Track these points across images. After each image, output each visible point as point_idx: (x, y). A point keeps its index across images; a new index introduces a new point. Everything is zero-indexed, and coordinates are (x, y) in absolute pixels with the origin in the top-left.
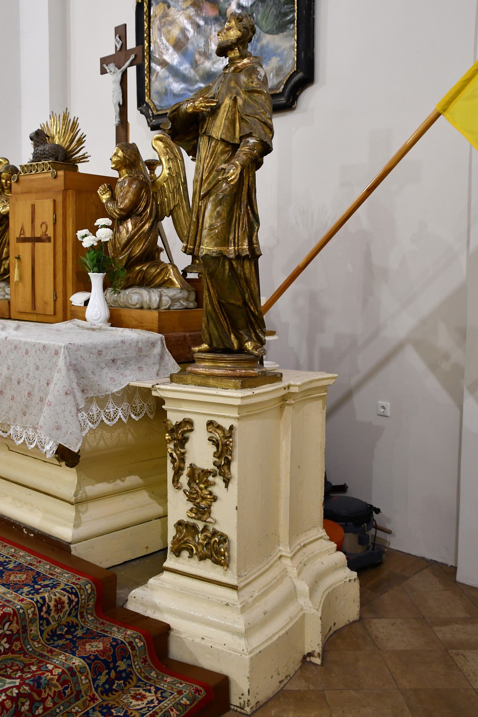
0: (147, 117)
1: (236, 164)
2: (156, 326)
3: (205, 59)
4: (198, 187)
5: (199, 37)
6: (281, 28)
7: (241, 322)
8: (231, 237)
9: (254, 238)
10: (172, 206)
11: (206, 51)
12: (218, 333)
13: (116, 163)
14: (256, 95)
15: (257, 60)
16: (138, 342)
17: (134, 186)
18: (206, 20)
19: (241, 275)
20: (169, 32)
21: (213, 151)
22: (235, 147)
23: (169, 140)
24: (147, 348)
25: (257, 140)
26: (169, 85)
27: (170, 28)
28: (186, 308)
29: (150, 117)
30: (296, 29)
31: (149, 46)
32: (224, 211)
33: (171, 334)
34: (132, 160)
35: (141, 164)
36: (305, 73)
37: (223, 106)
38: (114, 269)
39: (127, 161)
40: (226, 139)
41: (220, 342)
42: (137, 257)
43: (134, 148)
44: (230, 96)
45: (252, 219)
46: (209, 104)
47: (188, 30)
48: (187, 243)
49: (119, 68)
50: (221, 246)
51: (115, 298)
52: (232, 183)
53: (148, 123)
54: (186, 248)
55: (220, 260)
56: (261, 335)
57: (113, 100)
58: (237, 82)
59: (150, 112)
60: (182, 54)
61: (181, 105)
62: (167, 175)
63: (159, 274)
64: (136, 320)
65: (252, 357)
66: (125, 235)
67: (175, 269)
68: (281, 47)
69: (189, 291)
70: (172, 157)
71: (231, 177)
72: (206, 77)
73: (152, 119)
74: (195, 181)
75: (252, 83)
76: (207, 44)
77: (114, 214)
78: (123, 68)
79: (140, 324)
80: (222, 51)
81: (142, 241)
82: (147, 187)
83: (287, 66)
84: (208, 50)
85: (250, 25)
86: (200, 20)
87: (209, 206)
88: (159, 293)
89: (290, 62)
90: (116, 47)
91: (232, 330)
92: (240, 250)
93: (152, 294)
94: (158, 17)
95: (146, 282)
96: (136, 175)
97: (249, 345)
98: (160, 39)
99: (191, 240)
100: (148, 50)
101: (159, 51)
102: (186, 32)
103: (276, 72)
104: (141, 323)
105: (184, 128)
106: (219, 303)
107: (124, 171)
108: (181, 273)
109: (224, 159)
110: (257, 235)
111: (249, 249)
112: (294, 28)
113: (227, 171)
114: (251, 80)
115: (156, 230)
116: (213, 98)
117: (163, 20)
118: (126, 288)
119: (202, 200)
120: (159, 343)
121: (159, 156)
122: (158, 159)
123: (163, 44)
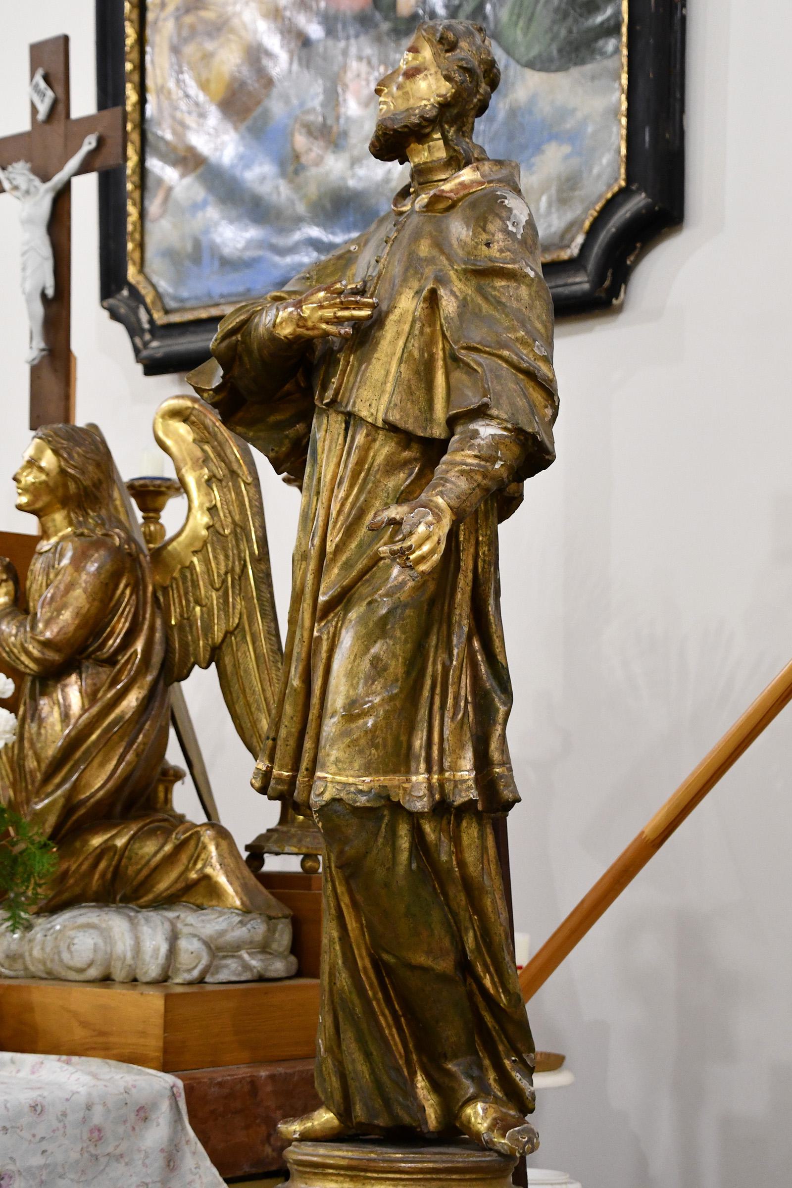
0: (134, 330)
1: (437, 507)
2: (153, 1044)
3: (327, 148)
4: (310, 578)
5: (307, 76)
6: (577, 49)
7: (452, 1032)
8: (418, 742)
9: (494, 745)
10: (218, 634)
11: (329, 122)
12: (373, 1072)
13: (33, 490)
14: (500, 283)
15: (504, 172)
16: (89, 1107)
17: (92, 567)
18: (330, 23)
19: (450, 870)
20: (207, 57)
21: (360, 463)
22: (432, 451)
23: (213, 419)
24: (121, 1129)
25: (505, 429)
26: (207, 231)
27: (209, 46)
28: (261, 979)
29: (143, 331)
30: (625, 52)
31: (142, 101)
32: (394, 656)
33: (204, 1074)
34: (87, 483)
35: (116, 494)
36: (654, 197)
37: (393, 317)
38: (14, 844)
39: (72, 487)
40: (401, 425)
41: (378, 1103)
42: (99, 803)
43: (94, 442)
44: (416, 285)
45: (489, 683)
46: (346, 313)
47: (269, 54)
48: (272, 760)
49: (45, 178)
50: (386, 773)
51: (14, 947)
52: (423, 567)
53: (137, 351)
54: (267, 775)
55: (383, 816)
56: (517, 1076)
57: (24, 279)
58: (440, 244)
59: (143, 316)
60: (250, 130)
61: (254, 313)
62: (204, 533)
63: (171, 859)
64: (84, 1024)
65: (489, 1158)
66: (58, 727)
67: (224, 844)
68: (574, 110)
69: (270, 918)
70: (220, 473)
71: (420, 546)
72: (328, 206)
73: (147, 337)
74: (299, 557)
75: (488, 245)
76: (333, 98)
77: (24, 658)
78: (59, 179)
79: (101, 1039)
80: (391, 143)
81: (113, 749)
82: (136, 570)
83: (595, 171)
84: (338, 118)
85: (481, 61)
86: (309, 21)
87: (347, 639)
88: (167, 925)
89: (605, 161)
90: (34, 110)
91: (420, 1061)
92: (448, 787)
93: (146, 930)
94: (171, 8)
95: (122, 889)
96: (99, 532)
97: (479, 1116)
98: (178, 81)
99: (284, 751)
100: (136, 116)
101: (173, 118)
102: (265, 61)
103: (560, 191)
104: (102, 1034)
105: (268, 388)
106: (377, 964)
107: (59, 517)
108: (245, 855)
109: (396, 489)
110: (503, 736)
111: (477, 780)
112: (617, 51)
113: (406, 528)
114: (484, 237)
115: (162, 708)
116: (362, 292)
117: (189, 19)
118: (53, 908)
119: (321, 619)
120: (165, 1106)
121: (178, 470)
122: (171, 474)
123: (187, 96)
